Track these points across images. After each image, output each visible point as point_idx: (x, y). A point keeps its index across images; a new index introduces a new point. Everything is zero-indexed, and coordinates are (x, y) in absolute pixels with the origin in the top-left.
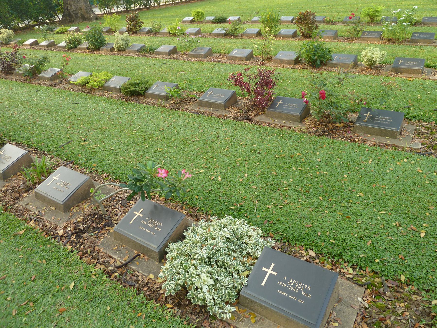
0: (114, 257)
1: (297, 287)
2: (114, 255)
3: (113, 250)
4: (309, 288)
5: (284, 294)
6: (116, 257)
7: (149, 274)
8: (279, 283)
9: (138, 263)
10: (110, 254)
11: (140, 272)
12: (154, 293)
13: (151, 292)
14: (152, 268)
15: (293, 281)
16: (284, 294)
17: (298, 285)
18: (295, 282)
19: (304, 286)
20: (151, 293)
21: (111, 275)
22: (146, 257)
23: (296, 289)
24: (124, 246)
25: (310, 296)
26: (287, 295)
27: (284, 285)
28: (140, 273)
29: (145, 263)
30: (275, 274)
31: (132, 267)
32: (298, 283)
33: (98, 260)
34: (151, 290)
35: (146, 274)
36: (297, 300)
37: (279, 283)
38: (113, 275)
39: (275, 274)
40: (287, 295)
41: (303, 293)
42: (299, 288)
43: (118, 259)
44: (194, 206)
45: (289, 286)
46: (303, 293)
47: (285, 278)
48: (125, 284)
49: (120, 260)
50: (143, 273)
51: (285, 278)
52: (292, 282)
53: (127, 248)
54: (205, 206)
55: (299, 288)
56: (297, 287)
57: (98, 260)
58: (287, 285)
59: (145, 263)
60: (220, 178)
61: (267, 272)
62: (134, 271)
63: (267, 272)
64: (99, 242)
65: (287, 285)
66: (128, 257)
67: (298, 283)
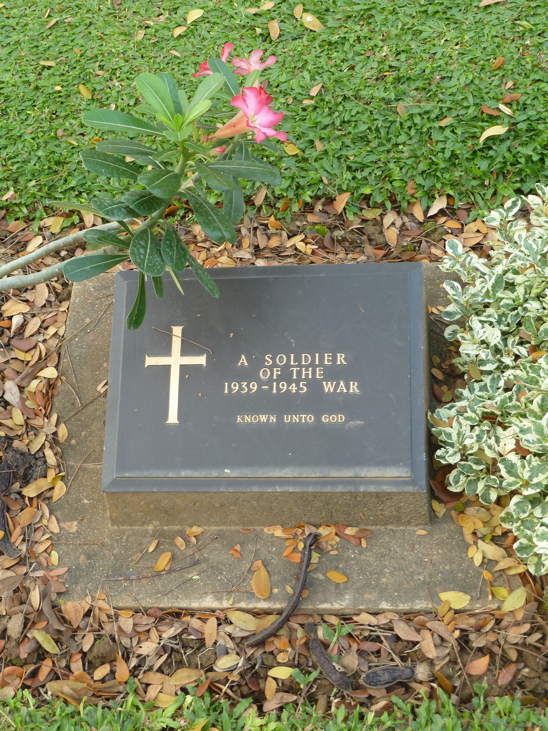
0: (195, 605)
1: (299, 373)
2: (187, 596)
3: (158, 574)
4: (341, 359)
5: (263, 418)
6: (209, 602)
7: (433, 596)
8: (230, 389)
9: (336, 577)
10: (166, 603)
11: (384, 605)
12: (531, 663)
13: (513, 668)
14: (420, 563)
15: (273, 359)
16: (263, 418)
17: (300, 366)
18: (282, 359)
19: (322, 358)
20: (519, 671)
21: (262, 693)
22: (349, 531)
23: (297, 385)
24: (196, 530)
25: (354, 387)
26: (273, 419)
27: (249, 389)
28: (383, 611)
29: (369, 557)
30: (201, 360)
31: (326, 606)
32: (298, 359)
33: (127, 659)
34: (506, 661)
35: (420, 605)
36: (280, 419)
37: (230, 389)
38: (270, 687)
39: (201, 360)
40: (273, 419)
41: (328, 387)
42: (307, 375)
43: (226, 604)
44: (317, 198)
45: (270, 381)
46: (328, 387)
47: (243, 360)
48: (362, 696)
49: (243, 605)
50: (403, 607)
51: (243, 360)
52: (274, 365)
53: (218, 537)
54: (366, 173)
55: (307, 375)
56: (299, 373)
57: (127, 659)
58: (260, 383)
59: (369, 557)
60: (309, 20)
61: (167, 369)
62: (345, 618)
63: (167, 369)
64: (54, 573)
65: (260, 383)
66: (263, 572)
67: (298, 359)
